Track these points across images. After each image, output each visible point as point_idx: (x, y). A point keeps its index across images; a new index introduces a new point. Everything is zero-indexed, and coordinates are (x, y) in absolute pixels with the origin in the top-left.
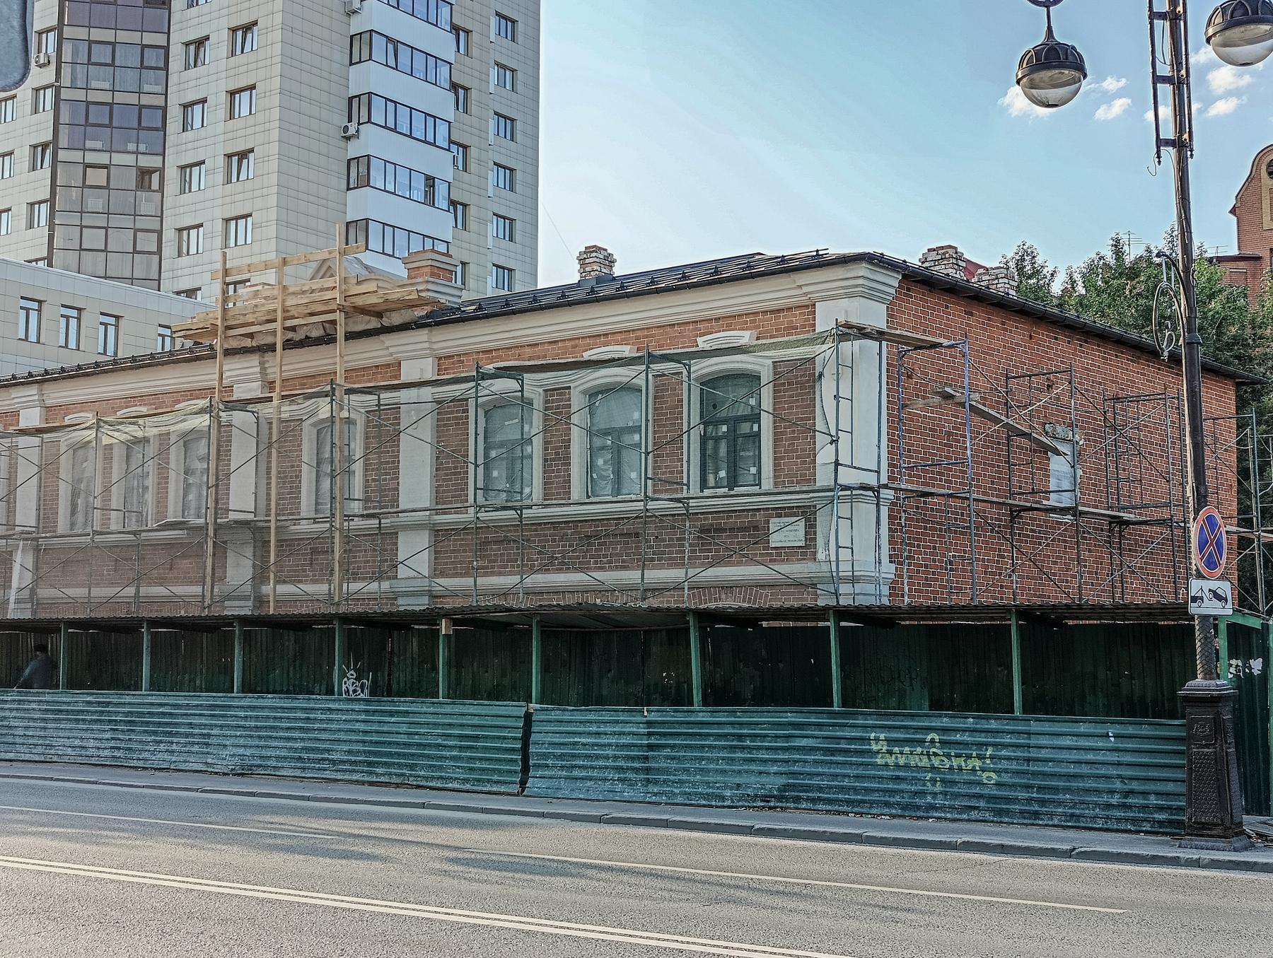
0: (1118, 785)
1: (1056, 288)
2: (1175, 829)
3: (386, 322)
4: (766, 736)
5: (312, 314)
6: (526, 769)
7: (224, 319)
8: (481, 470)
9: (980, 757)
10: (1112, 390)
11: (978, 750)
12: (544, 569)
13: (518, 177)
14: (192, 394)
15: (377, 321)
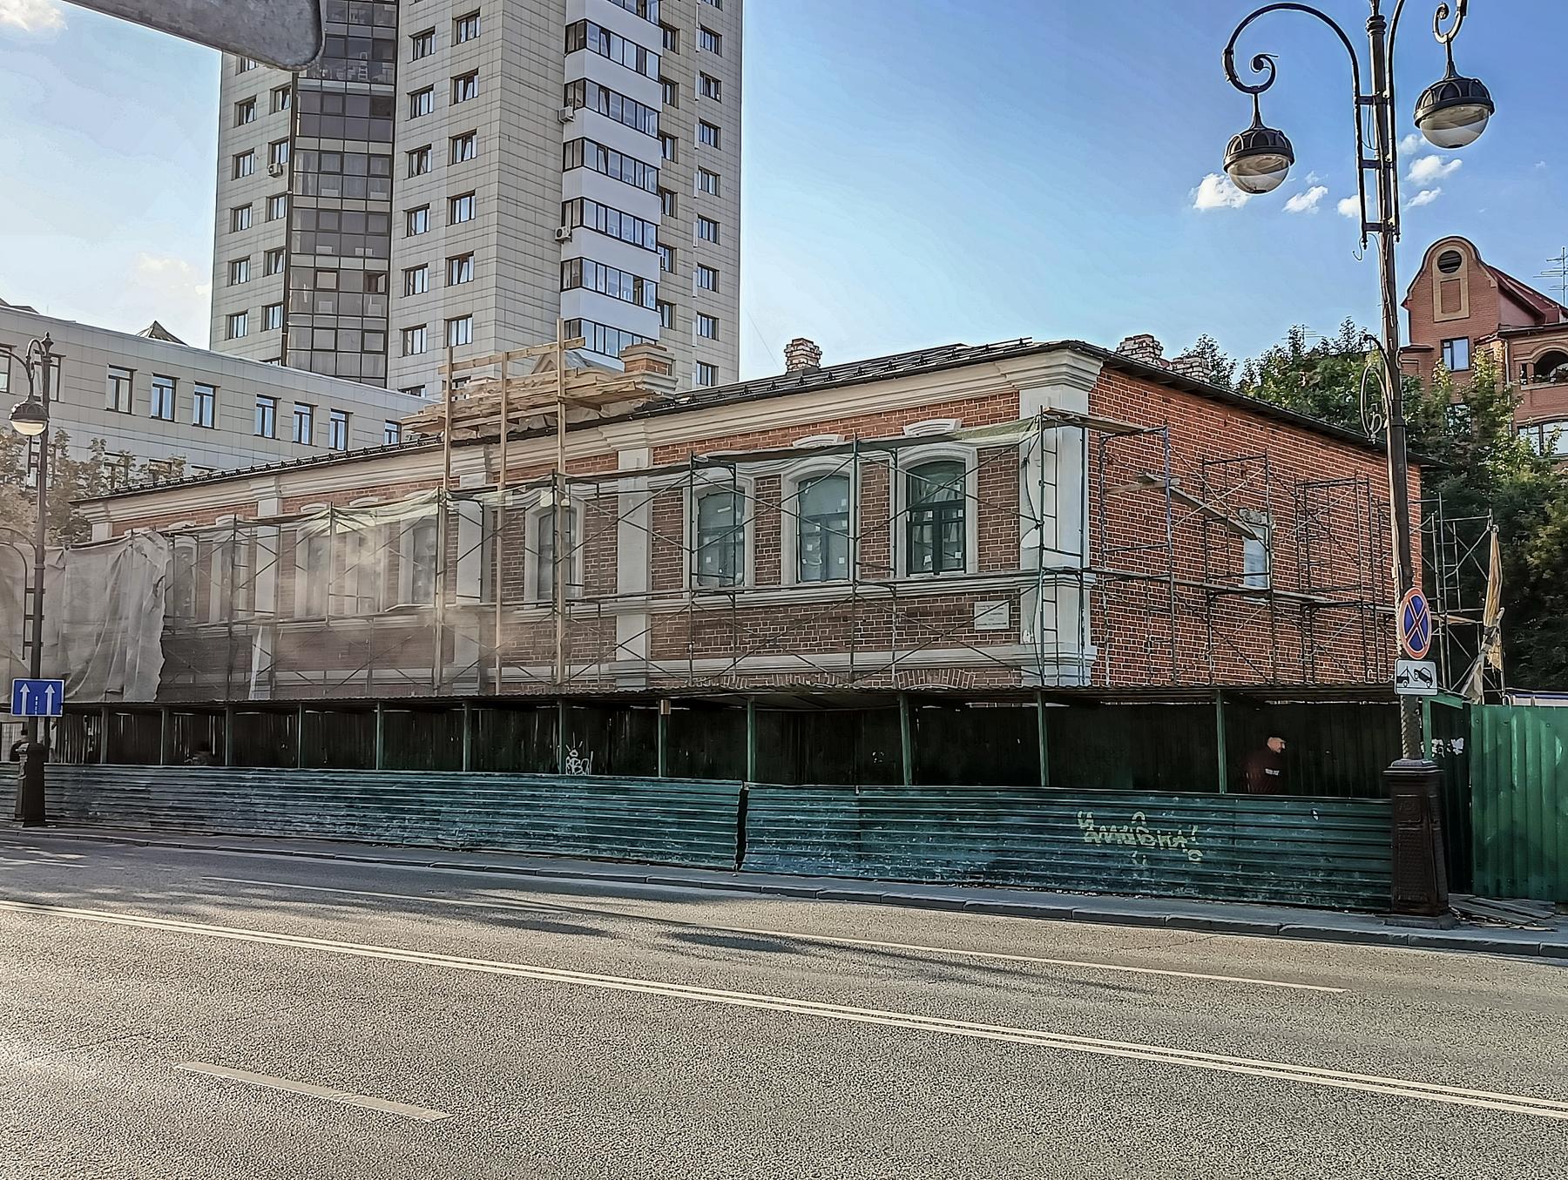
0: (1322, 862)
1: (1235, 380)
2: (1381, 907)
3: (604, 413)
4: (975, 814)
5: (534, 407)
6: (741, 846)
7: (451, 412)
8: (695, 555)
9: (1185, 835)
10: (1304, 475)
11: (1183, 832)
12: (756, 652)
13: (720, 277)
14: (422, 485)
15: (592, 412)
